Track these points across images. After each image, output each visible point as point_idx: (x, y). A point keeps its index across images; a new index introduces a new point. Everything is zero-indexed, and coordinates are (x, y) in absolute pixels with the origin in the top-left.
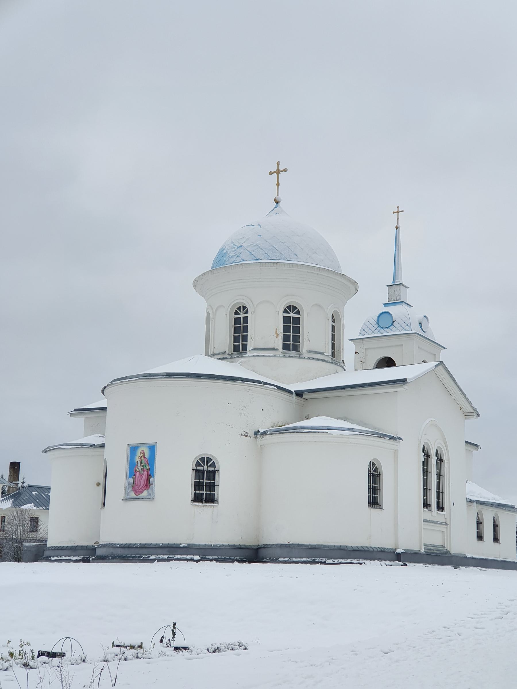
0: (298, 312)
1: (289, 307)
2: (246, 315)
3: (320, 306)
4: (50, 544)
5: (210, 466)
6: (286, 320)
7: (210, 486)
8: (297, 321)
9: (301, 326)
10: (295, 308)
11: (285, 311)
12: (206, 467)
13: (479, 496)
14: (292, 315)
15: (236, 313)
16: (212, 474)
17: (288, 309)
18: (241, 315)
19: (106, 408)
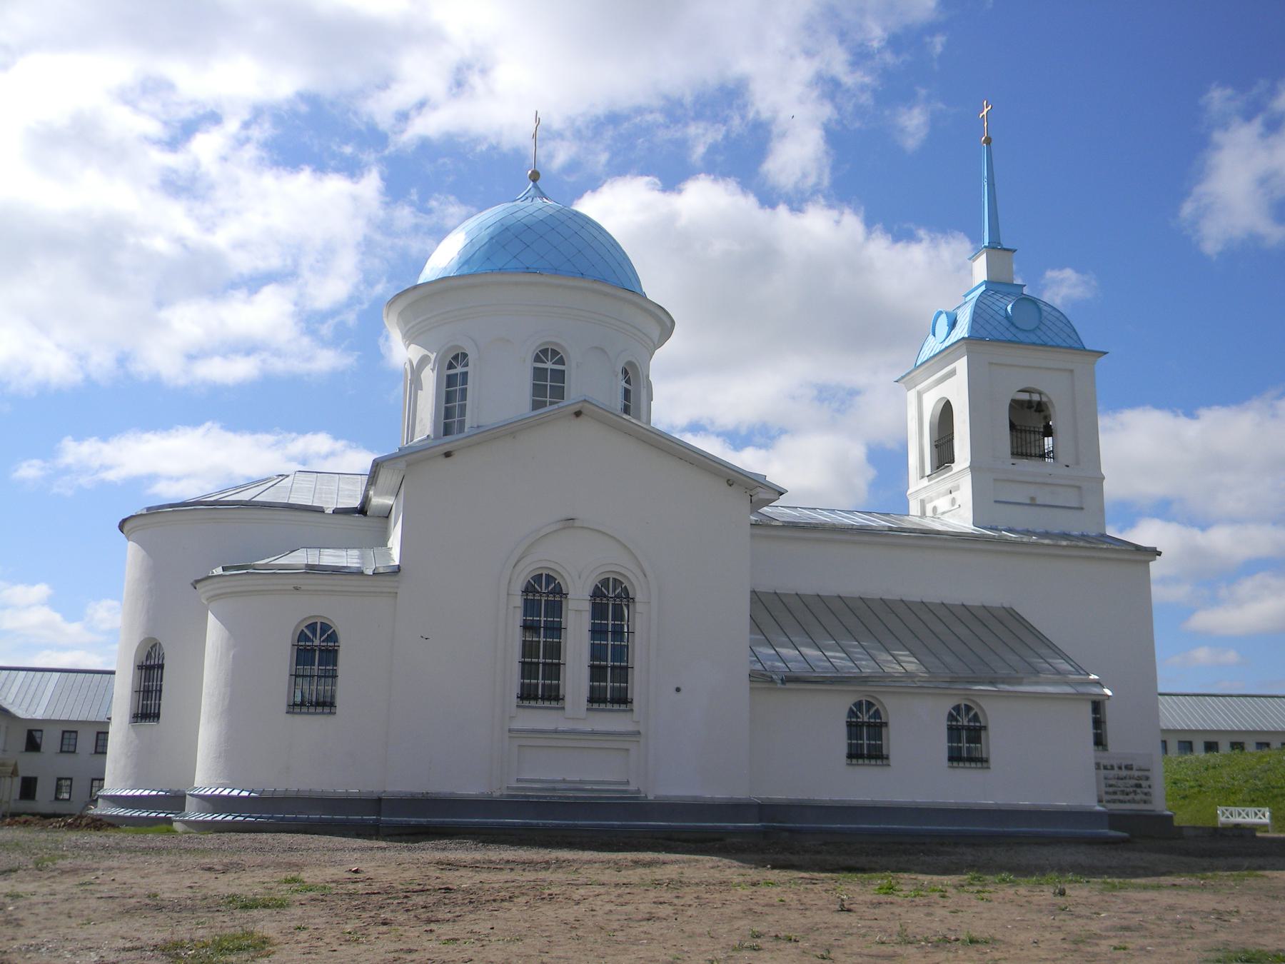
0: (561, 361)
1: (545, 352)
2: (465, 369)
3: (602, 350)
4: (836, 116)
5: (326, 640)
6: (539, 374)
7: (553, 629)
8: (559, 376)
9: (566, 385)
10: (555, 353)
11: (537, 359)
12: (317, 642)
13: (689, 895)
14: (549, 365)
15: (451, 366)
16: (330, 655)
17: (543, 354)
18: (459, 370)
19: (113, 673)
